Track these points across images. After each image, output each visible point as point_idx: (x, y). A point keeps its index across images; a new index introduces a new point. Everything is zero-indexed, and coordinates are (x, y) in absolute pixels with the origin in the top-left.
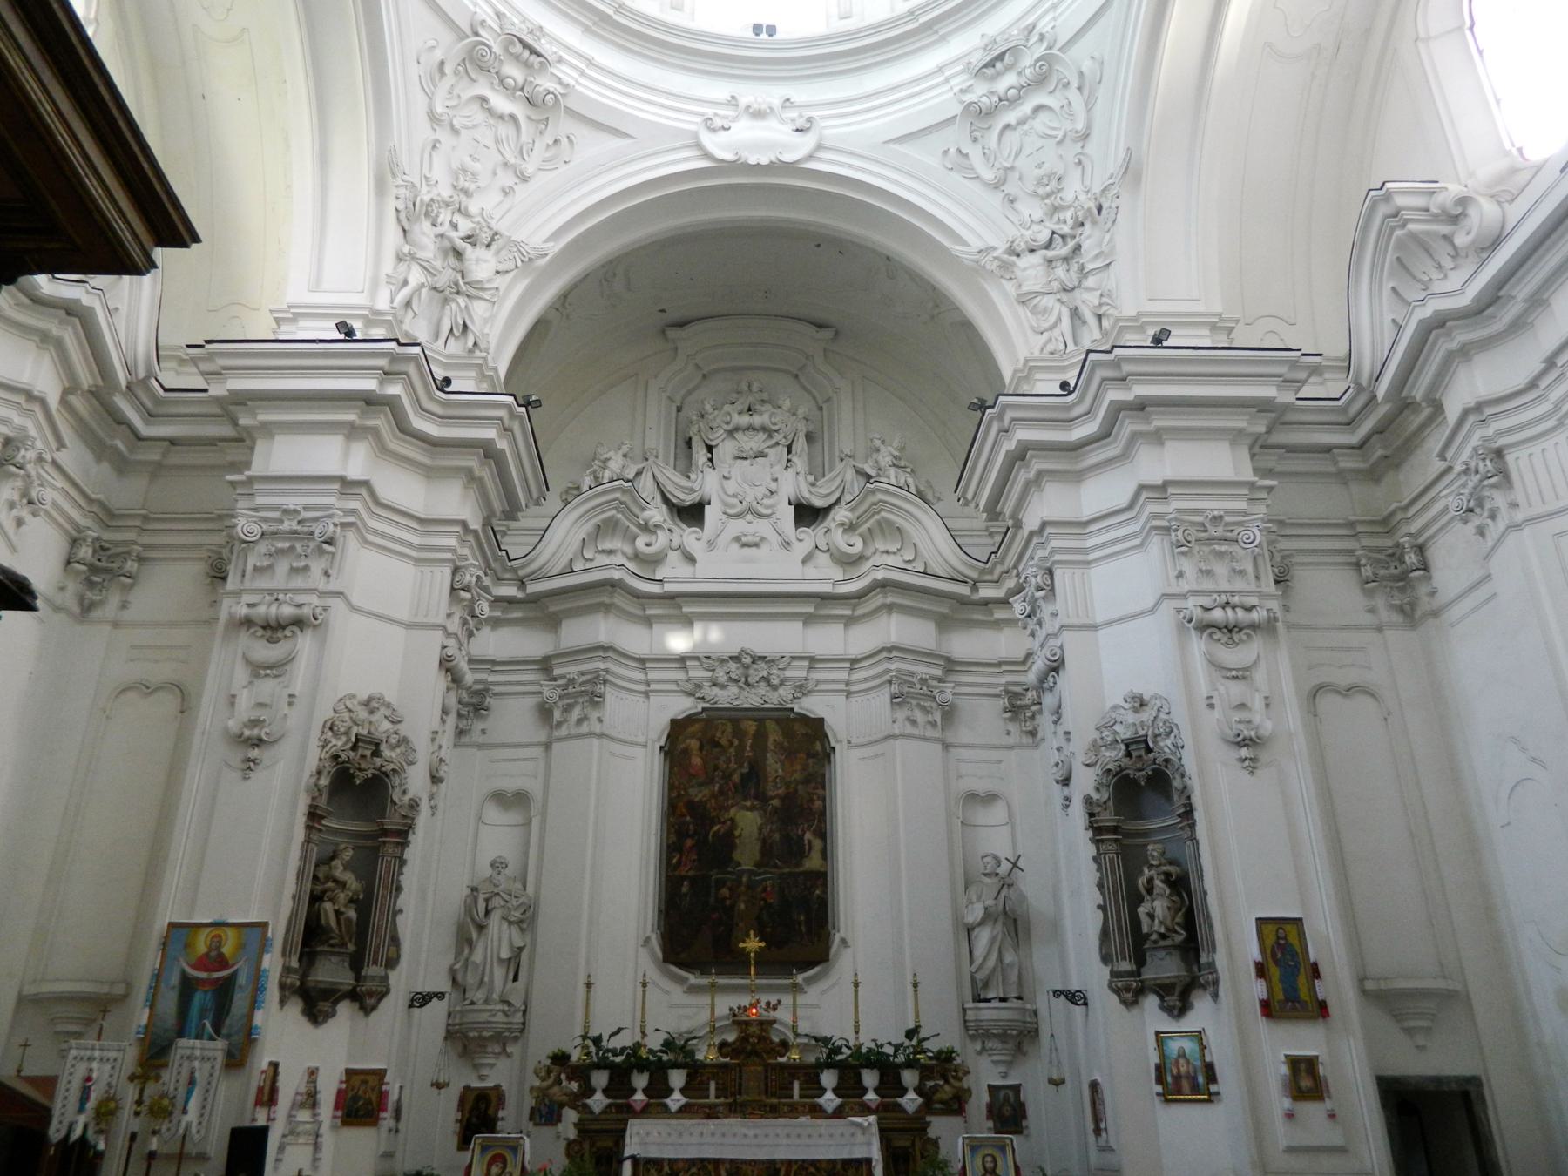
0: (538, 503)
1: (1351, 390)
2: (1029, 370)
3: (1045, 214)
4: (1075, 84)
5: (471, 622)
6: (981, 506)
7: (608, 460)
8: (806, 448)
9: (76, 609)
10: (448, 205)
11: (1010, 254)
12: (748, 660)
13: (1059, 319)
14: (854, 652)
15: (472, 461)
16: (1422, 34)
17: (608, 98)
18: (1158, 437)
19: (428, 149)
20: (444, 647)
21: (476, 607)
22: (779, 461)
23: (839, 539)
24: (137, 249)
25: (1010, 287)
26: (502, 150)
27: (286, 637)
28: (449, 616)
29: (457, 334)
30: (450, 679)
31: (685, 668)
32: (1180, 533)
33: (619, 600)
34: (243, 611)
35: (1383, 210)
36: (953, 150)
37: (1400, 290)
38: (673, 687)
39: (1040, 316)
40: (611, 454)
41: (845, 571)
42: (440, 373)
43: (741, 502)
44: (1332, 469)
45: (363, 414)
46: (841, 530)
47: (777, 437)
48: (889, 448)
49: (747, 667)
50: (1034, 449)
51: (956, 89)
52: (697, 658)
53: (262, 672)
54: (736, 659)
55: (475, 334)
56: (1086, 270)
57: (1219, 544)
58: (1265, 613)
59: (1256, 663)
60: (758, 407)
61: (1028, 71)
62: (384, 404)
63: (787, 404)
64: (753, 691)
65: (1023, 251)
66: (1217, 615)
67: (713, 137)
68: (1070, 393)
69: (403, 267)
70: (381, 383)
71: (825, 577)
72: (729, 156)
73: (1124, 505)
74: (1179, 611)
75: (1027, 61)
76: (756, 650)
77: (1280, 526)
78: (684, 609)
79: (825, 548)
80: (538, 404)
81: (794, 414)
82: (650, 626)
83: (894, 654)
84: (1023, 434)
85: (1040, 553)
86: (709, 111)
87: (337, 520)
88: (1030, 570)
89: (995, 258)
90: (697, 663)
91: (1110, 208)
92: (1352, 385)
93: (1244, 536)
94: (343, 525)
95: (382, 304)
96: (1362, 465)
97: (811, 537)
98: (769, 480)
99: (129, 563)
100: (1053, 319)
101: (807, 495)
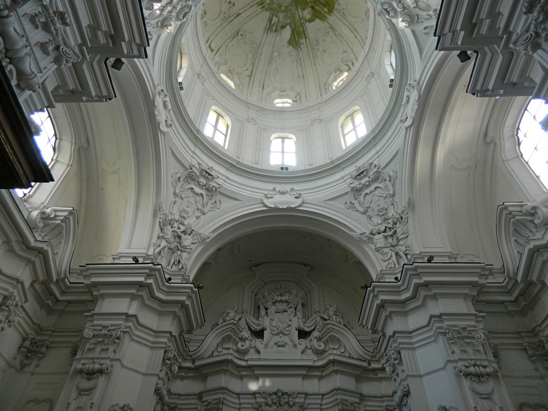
0: (201, 328)
1: (507, 279)
2: (382, 274)
3: (382, 221)
4: (388, 179)
5: (169, 374)
6: (369, 327)
7: (229, 313)
8: (302, 308)
9: (18, 367)
10: (177, 221)
11: (371, 235)
12: (280, 394)
13: (391, 256)
14: (323, 391)
15: (176, 309)
16: (505, 159)
17: (234, 189)
18: (435, 297)
19: (173, 203)
20: (157, 384)
21: (172, 368)
22: (292, 313)
23: (315, 343)
24: (24, 178)
25: (372, 246)
26: (197, 204)
27: (94, 378)
28: (161, 370)
29: (176, 263)
30: (158, 398)
31: (255, 398)
32: (450, 334)
33: (230, 368)
34: (80, 366)
35: (505, 212)
36: (348, 202)
37: (518, 240)
38: (250, 406)
39: (384, 256)
40: (230, 311)
41: (318, 357)
42: (167, 277)
43: (278, 329)
44: (505, 310)
45: (138, 290)
46: (316, 340)
47: (291, 305)
48: (333, 308)
49: (280, 397)
50: (388, 303)
51: (348, 183)
52: (260, 393)
53: (82, 393)
54: (275, 394)
55: (182, 264)
56: (399, 239)
57: (467, 339)
58: (492, 369)
59: (493, 391)
60: (284, 294)
61: (372, 176)
62: (145, 286)
63: (295, 293)
64: (282, 408)
65: (376, 233)
66: (472, 369)
67: (267, 200)
68: (399, 281)
69: (160, 240)
70: (146, 279)
71: (310, 359)
72: (273, 206)
73: (426, 324)
74: (455, 368)
75: (371, 173)
76: (283, 390)
77: (490, 333)
78: (256, 372)
79: (310, 347)
80: (202, 288)
81: (297, 296)
82: (242, 379)
83: (339, 391)
84: (382, 297)
85: (394, 345)
86: (266, 192)
87: (122, 330)
88: (391, 352)
89: (366, 236)
90: (260, 395)
91: (405, 217)
92: (507, 277)
93: (477, 335)
94: (124, 332)
95: (151, 252)
96: (517, 309)
97: (304, 343)
98: (288, 321)
99: (43, 348)
100: (389, 256)
101: (302, 327)
